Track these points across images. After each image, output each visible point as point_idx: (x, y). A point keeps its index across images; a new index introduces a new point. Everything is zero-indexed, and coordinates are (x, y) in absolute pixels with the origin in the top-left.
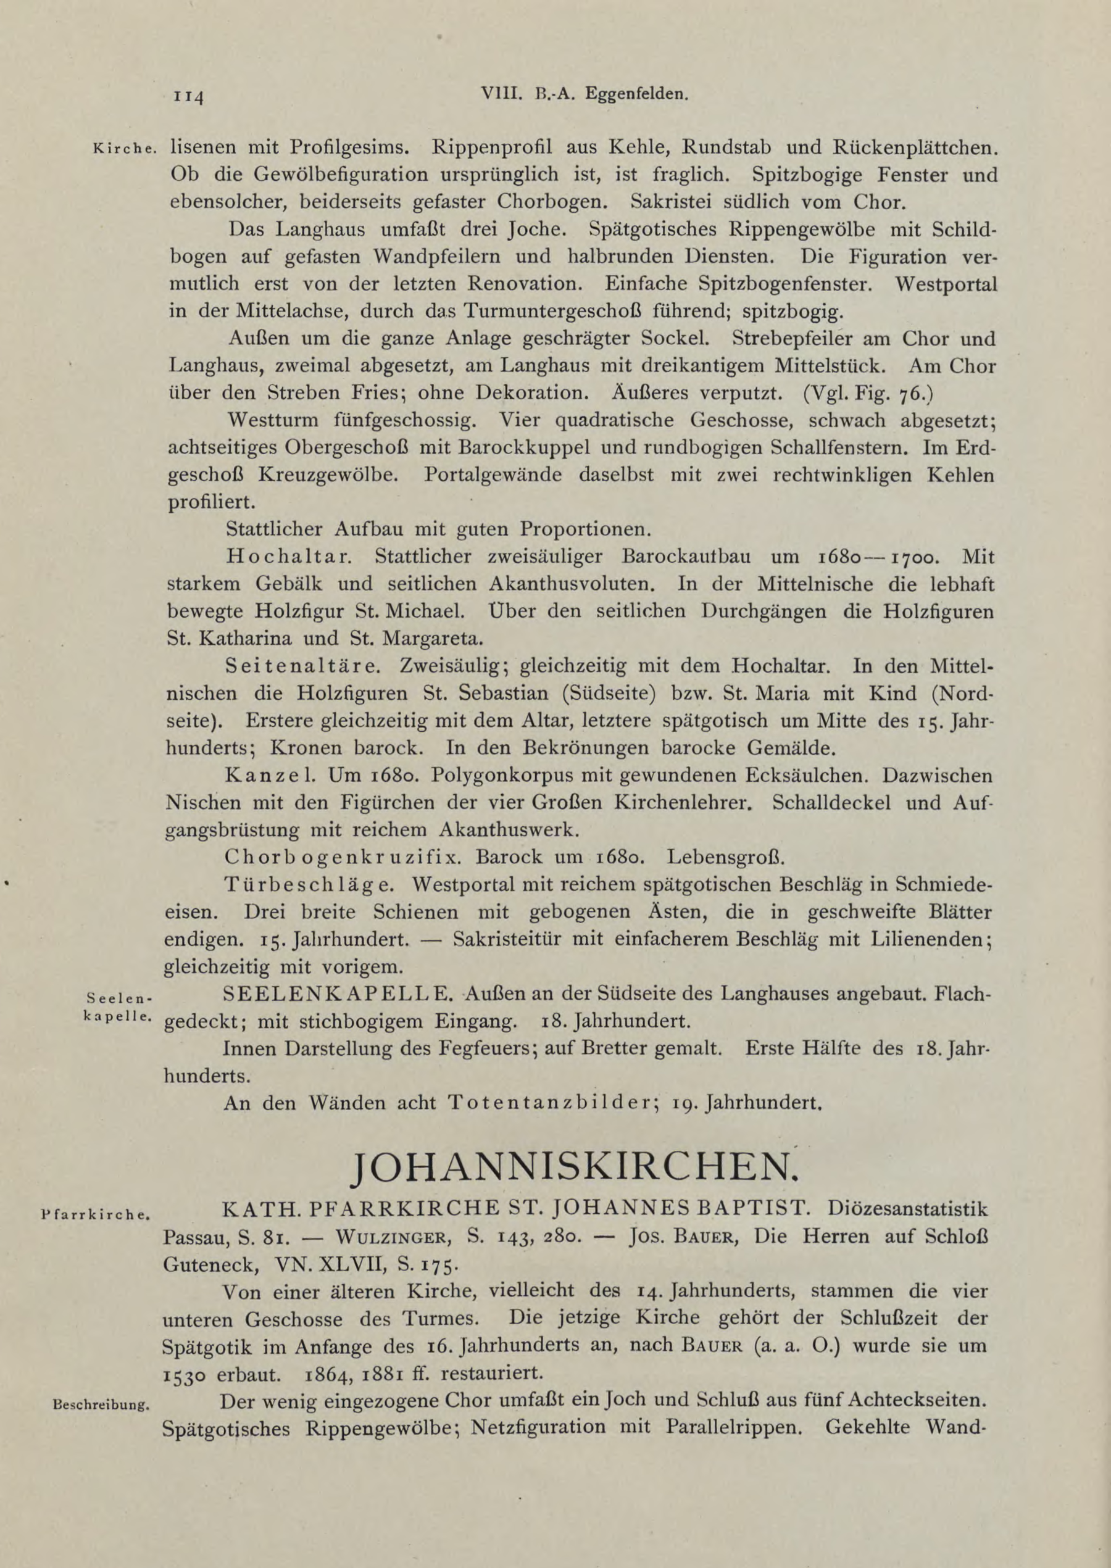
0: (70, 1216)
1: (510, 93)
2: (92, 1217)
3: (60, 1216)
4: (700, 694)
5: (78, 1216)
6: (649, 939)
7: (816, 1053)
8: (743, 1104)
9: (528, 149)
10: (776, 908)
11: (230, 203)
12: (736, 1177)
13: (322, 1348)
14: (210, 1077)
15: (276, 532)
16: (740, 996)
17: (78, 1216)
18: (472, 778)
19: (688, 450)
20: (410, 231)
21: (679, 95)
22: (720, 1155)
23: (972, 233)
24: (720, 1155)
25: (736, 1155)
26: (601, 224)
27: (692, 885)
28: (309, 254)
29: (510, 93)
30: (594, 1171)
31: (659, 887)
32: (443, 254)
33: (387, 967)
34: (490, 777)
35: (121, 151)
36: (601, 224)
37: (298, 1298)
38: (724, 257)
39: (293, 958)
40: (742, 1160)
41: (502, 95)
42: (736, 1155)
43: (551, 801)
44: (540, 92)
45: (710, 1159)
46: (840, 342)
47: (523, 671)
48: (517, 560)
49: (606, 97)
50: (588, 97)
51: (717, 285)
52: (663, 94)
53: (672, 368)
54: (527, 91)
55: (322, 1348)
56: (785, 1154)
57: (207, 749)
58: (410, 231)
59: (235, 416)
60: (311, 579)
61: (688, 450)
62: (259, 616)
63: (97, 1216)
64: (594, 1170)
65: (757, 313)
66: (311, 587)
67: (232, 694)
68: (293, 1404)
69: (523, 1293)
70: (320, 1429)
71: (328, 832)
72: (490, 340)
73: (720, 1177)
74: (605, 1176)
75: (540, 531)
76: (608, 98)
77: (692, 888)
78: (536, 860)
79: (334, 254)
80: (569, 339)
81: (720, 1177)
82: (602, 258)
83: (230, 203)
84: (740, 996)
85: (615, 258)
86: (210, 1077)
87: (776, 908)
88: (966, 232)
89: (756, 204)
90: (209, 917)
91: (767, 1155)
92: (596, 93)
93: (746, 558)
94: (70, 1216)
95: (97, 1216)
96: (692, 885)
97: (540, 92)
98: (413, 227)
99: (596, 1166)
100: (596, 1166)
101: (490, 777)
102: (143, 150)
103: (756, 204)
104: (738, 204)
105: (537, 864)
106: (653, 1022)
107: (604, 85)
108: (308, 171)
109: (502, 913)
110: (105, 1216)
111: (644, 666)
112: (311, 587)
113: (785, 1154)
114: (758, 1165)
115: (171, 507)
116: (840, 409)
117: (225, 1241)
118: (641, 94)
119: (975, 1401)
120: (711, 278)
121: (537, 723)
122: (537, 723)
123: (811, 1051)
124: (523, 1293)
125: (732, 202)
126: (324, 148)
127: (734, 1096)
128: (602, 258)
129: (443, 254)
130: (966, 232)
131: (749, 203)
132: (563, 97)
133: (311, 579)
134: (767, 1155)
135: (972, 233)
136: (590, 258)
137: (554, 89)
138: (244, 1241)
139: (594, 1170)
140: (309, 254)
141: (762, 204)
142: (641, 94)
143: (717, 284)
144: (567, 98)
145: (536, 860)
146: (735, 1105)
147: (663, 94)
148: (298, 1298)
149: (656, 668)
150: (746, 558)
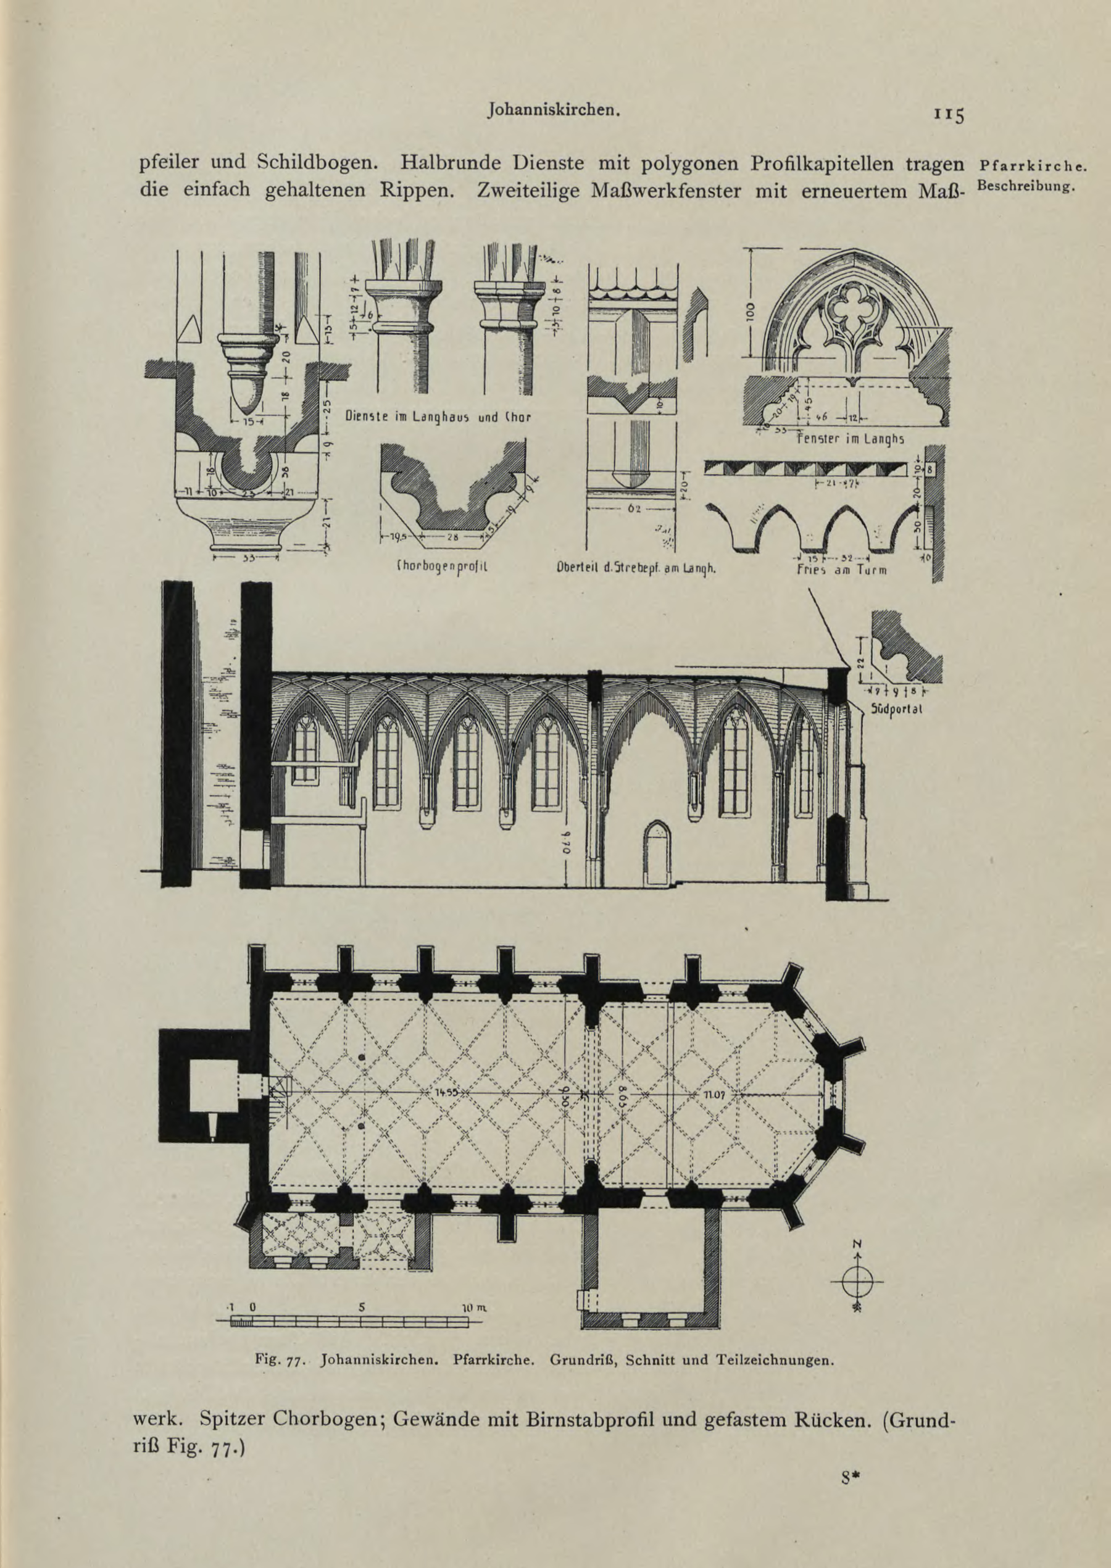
0: (1009, 167)
2: (1030, 168)
3: (998, 166)
5: (1017, 168)
7: (414, 167)
9: (778, 165)
11: (659, 165)
13: (212, 190)
17: (1017, 168)
18: (681, 167)
19: (315, 165)
23: (297, 165)
27: (692, 164)
28: (729, 1417)
32: (154, 160)
34: (699, 165)
35: (1051, 168)
37: (231, 166)
38: (552, 164)
46: (877, 167)
55: (212, 190)
57: (485, 164)
60: (802, 159)
61: (315, 165)
62: (405, 167)
63: (1036, 167)
65: (831, 166)
66: (802, 167)
67: (888, 165)
69: (866, 167)
70: (395, 191)
71: (616, 165)
72: (931, 166)
75: (770, 165)
77: (692, 167)
79: (570, 161)
80: (285, 163)
82: (442, 164)
83: (659, 165)
85: (454, 164)
88: (291, 165)
93: (579, 164)
94: (1009, 167)
95: (1036, 167)
96: (692, 164)
101: (699, 165)
102: (1074, 168)
109: (623, 164)
110: (1044, 167)
111: (604, 163)
112: (802, 167)
115: (142, 168)
119: (367, 163)
123: (409, 165)
124: (866, 167)
126: (785, 164)
128: (442, 164)
129: (154, 160)
130: (291, 165)
131: (309, 164)
133: (802, 159)
135: (297, 165)
136: (429, 164)
140: (729, 1417)
149: (616, 166)
150: (579, 164)
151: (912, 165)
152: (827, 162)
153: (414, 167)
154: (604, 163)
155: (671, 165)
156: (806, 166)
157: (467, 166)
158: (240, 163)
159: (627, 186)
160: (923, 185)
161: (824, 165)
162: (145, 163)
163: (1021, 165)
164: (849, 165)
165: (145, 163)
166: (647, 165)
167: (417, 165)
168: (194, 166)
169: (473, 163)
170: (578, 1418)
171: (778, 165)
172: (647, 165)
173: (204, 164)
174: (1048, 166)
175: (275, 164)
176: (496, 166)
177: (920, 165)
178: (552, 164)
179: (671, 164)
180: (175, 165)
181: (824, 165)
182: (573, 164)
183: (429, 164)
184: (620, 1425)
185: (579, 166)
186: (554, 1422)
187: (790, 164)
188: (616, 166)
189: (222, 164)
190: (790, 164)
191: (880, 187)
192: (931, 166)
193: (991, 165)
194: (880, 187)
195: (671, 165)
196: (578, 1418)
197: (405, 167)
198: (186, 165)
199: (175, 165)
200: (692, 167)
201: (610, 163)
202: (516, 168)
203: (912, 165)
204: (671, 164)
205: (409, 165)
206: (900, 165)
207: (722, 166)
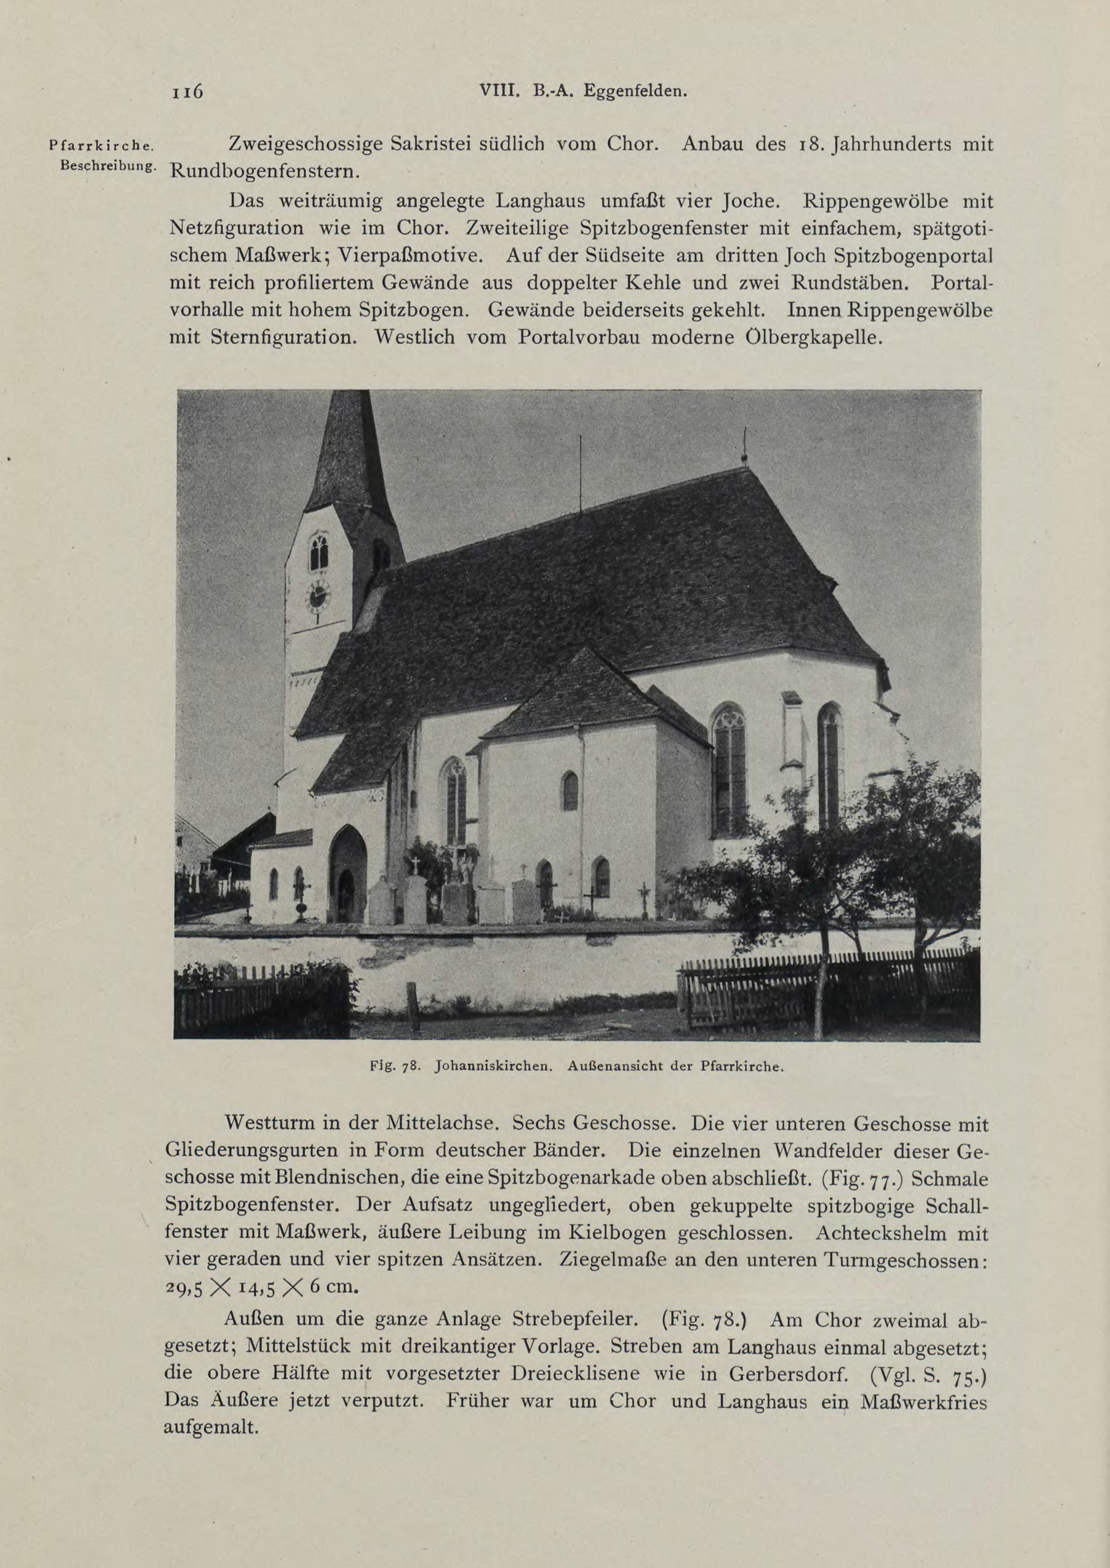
0: (77, 147)
1: (506, 89)
3: (66, 147)
4: (285, 202)
5: (85, 148)
7: (285, 1378)
9: (291, 284)
10: (705, 1370)
11: (306, 312)
14: (221, 170)
15: (428, 340)
17: (85, 148)
19: (221, 174)
21: (677, 92)
26: (846, 251)
27: (961, 229)
29: (506, 89)
35: (119, 148)
36: (846, 251)
37: (310, 1264)
39: (264, 301)
41: (507, 88)
44: (539, 90)
46: (722, 1263)
48: (262, 147)
49: (605, 94)
50: (587, 95)
51: (598, 230)
52: (661, 91)
54: (525, 88)
57: (452, 284)
62: (276, 1377)
63: (104, 147)
68: (264, 1207)
69: (861, 341)
76: (609, 95)
77: (961, 232)
80: (939, 1180)
85: (234, 1152)
86: (221, 170)
87: (705, 1370)
89: (512, 147)
90: (534, 1264)
92: (595, 90)
94: (77, 147)
95: (104, 147)
96: (961, 229)
97: (539, 90)
98: (633, 199)
101: (968, 230)
102: (141, 147)
103: (512, 147)
104: (494, 147)
107: (603, 82)
108: (920, 198)
110: (112, 147)
111: (257, 310)
118: (641, 92)
119: (458, 311)
120: (592, 223)
123: (280, 1375)
124: (861, 341)
125: (488, 144)
131: (505, 146)
132: (561, 94)
137: (552, 85)
141: (518, 147)
142: (641, 92)
143: (598, 228)
144: (565, 94)
147: (661, 91)
148: (310, 1264)
152: (835, 335)
153: (285, 1378)
154: (658, 338)
158: (721, 285)
159: (270, 250)
161: (832, 339)
169: (307, 1259)
171: (291, 284)
173: (814, 1403)
175: (929, 1181)
177: (255, 229)
178: (188, 1232)
179: (575, 337)
180: (608, 1322)
181: (832, 339)
182: (322, 173)
183: (222, 311)
184: (546, 342)
189: (301, 1261)
190: (302, 283)
191: (347, 279)
192: (573, 1348)
193: (59, 146)
194: (347, 279)
197: (276, 1377)
198: (869, 1154)
199: (608, 1322)
200: (961, 232)
202: (632, 1155)
204: (575, 337)
205: (280, 1375)
207: (513, 1153)
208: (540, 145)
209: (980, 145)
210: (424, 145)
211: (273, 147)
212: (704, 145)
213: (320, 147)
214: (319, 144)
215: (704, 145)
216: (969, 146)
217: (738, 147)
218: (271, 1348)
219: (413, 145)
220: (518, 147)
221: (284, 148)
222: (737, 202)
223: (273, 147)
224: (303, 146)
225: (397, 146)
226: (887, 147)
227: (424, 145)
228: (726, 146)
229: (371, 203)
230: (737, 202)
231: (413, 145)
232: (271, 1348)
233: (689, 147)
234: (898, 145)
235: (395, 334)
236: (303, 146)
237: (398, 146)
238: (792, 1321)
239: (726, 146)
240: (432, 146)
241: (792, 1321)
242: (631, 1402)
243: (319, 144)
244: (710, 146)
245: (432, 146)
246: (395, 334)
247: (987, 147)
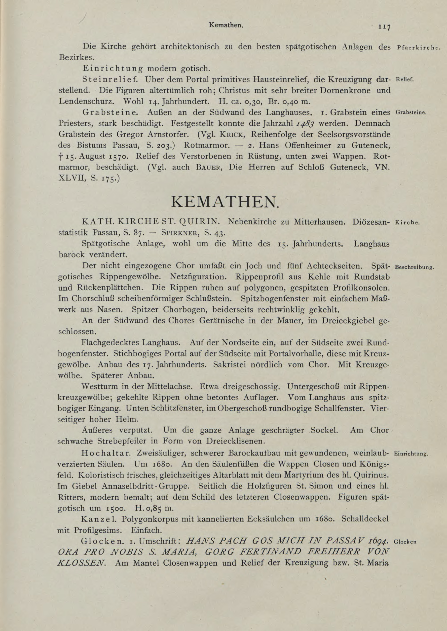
0: (408, 48)
3: (404, 48)
5: (412, 48)
6: (344, 299)
8: (177, 102)
9: (344, 288)
11: (251, 288)
12: (255, 206)
16: (361, 245)
17: (412, 48)
18: (138, 521)
19: (287, 409)
20: (211, 267)
22: (248, 197)
23: (208, 498)
24: (248, 197)
25: (255, 197)
30: (176, 204)
31: (379, 267)
33: (368, 124)
34: (267, 288)
40: (257, 199)
42: (255, 197)
43: (167, 485)
45: (244, 199)
47: (118, 400)
53: (262, 135)
56: (274, 197)
58: (211, 267)
59: (126, 100)
62: (224, 99)
63: (420, 48)
64: (175, 203)
66: (354, 289)
69: (72, 91)
71: (356, 355)
73: (248, 206)
74: (180, 206)
75: (341, 288)
77: (264, 289)
78: (82, 256)
81: (248, 206)
83: (251, 288)
84: (361, 245)
88: (205, 498)
89: (269, 366)
91: (267, 197)
93: (379, 91)
95: (420, 48)
99: (176, 202)
100: (176, 202)
101: (267, 288)
102: (414, 223)
103: (269, 366)
105: (82, 258)
106: (194, 102)
109: (263, 354)
111: (257, 91)
113: (274, 197)
114: (263, 201)
116: (213, 141)
117: (137, 147)
119: (326, 497)
121: (219, 476)
122: (219, 476)
123: (263, 146)
124: (72, 91)
126: (276, 277)
127: (304, 241)
130: (205, 498)
134: (267, 197)
135: (208, 498)
138: (149, 146)
139: (175, 203)
141: (271, 366)
145: (82, 256)
146: (305, 245)
150: (379, 91)
151: (129, 476)
153: (265, 147)
155: (256, 288)
156: (350, 91)
157: (227, 564)
158: (234, 564)
160: (279, 318)
161: (199, 563)
162: (215, 80)
163: (413, 48)
164: (254, 343)
165: (215, 80)
166: (246, 288)
167: (266, 146)
168: (329, 147)
169: (189, 102)
170: (379, 276)
172: (246, 288)
173: (197, 266)
174: (405, 222)
176: (258, 125)
177: (204, 277)
181: (199, 563)
185: (242, 124)
186: (111, 387)
187: (89, 530)
188: (230, 81)
189: (187, 102)
190: (89, 530)
192: (359, 48)
193: (402, 47)
195: (256, 288)
196: (379, 276)
197: (224, 99)
201: (318, 299)
203: (129, 476)
204: (134, 519)
205: (263, 146)
206: (179, 430)
208: (217, 47)
209: (291, 453)
210: (227, 365)
211: (238, 388)
212: (237, 431)
213: (238, 322)
214: (256, 387)
215: (237, 431)
216: (301, 520)
217: (278, 454)
218: (242, 245)
219: (222, 365)
220: (271, 366)
221: (242, 388)
222: (251, 267)
223: (238, 388)
224: (320, 387)
225: (216, 366)
226: (179, 366)
227: (227, 365)
228: (420, 113)
229: (379, 465)
230: (251, 267)
231: (222, 365)
232: (242, 245)
233: (184, 465)
234: (320, 244)
235: (186, 155)
236: (320, 387)
237: (101, 465)
238: (359, 430)
239: (420, 113)
240: (232, 91)
241: (359, 430)
242: (317, 365)
243: (256, 387)
244: (133, 355)
245: (232, 91)
246: (186, 155)
247: (294, 454)
